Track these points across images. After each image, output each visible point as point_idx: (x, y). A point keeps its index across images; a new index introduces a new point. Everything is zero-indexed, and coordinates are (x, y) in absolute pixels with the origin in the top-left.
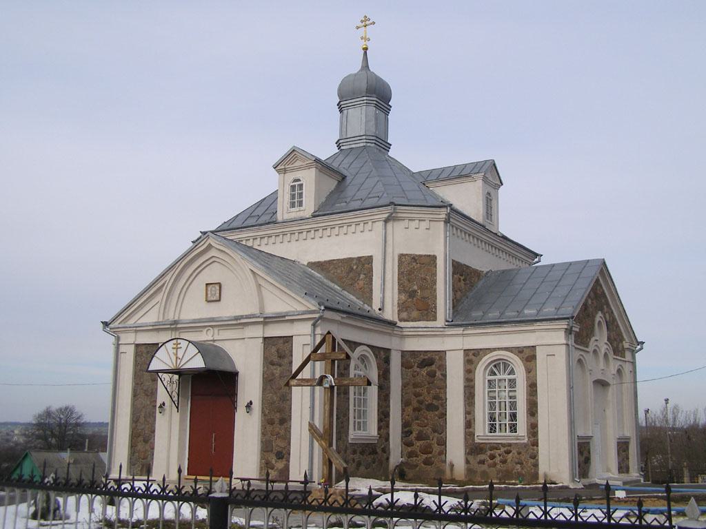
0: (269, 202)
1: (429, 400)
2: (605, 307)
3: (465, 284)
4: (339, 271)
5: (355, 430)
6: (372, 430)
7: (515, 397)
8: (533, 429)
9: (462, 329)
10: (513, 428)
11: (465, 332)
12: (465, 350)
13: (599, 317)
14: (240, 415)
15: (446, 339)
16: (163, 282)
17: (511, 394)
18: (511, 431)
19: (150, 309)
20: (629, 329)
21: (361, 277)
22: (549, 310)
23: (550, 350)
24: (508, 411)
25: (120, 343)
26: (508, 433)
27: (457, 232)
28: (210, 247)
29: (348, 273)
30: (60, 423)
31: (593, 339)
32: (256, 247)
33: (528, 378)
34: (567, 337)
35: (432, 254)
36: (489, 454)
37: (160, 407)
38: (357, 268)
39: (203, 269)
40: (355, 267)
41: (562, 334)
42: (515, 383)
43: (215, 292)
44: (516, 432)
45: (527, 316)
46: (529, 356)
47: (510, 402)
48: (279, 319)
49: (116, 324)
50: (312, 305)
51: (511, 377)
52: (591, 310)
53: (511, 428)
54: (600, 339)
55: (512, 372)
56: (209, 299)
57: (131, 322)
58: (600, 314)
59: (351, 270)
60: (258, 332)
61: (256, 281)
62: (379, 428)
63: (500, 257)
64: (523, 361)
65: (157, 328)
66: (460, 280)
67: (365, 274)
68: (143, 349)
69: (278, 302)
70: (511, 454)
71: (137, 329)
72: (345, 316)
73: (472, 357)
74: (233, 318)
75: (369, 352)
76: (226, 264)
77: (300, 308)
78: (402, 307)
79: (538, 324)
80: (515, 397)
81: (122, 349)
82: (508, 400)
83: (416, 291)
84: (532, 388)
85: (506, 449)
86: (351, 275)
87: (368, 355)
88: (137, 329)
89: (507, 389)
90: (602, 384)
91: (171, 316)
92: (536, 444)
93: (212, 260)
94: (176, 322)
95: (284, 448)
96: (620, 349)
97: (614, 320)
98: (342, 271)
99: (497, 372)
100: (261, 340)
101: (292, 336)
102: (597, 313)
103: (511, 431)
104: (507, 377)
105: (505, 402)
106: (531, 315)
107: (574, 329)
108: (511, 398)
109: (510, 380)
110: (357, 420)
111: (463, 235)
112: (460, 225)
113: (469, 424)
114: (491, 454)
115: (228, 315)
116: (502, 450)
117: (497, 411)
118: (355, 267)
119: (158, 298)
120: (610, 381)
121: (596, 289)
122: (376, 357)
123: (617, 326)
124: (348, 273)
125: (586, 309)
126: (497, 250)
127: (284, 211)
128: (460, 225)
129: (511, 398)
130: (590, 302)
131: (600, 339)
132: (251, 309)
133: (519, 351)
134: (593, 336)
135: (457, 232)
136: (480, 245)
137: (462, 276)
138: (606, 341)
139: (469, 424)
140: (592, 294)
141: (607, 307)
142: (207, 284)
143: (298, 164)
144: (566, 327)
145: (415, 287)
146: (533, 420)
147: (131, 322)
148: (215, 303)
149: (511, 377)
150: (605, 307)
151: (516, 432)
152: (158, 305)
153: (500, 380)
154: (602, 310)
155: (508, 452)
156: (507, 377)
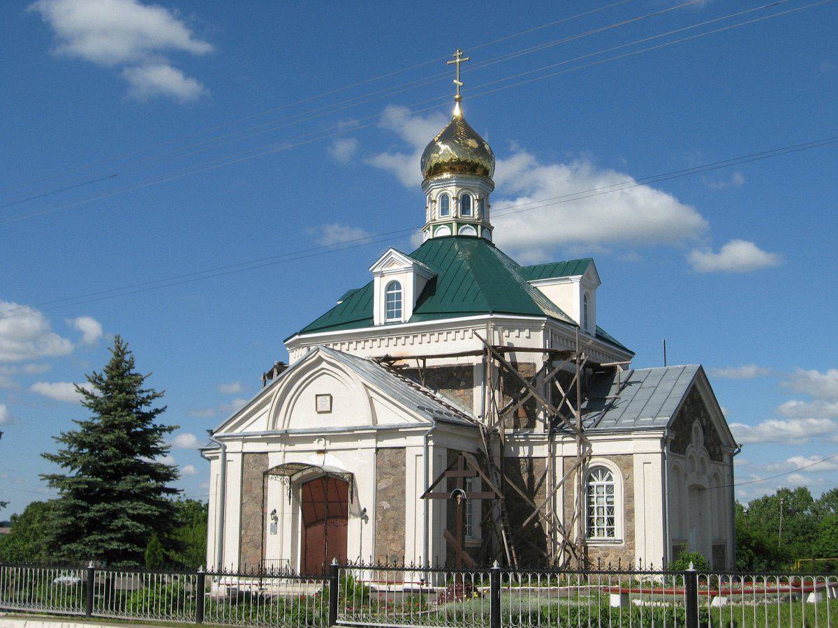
1: (686, 557)
7: (612, 503)
8: (630, 535)
9: (562, 436)
10: (611, 532)
11: (565, 439)
12: (564, 457)
13: (696, 424)
14: (353, 524)
16: (271, 392)
17: (609, 500)
18: (609, 535)
19: (257, 419)
20: (713, 400)
22: (646, 420)
24: (606, 516)
25: (226, 451)
26: (606, 537)
27: (567, 343)
28: (320, 360)
32: (343, 351)
33: (626, 485)
34: (662, 447)
35: (531, 361)
37: (272, 514)
38: (457, 375)
41: (658, 442)
42: (613, 488)
43: (326, 403)
44: (613, 536)
45: (623, 425)
46: (625, 462)
47: (608, 507)
48: (392, 432)
49: (222, 433)
50: (426, 419)
51: (609, 483)
53: (608, 532)
54: (696, 447)
55: (610, 478)
56: (319, 410)
57: (237, 431)
60: (372, 443)
61: (368, 393)
64: (620, 468)
65: (266, 438)
67: (465, 381)
68: (250, 459)
69: (390, 415)
70: (609, 557)
71: (245, 439)
72: (453, 427)
74: (346, 429)
76: (341, 379)
77: (413, 421)
79: (636, 433)
80: (612, 503)
81: (229, 457)
82: (606, 505)
84: (629, 497)
88: (245, 439)
89: (605, 495)
90: (699, 489)
91: (280, 426)
92: (632, 547)
93: (322, 373)
94: (287, 432)
95: (399, 552)
96: (717, 453)
97: (711, 424)
98: (442, 377)
99: (595, 478)
100: (374, 450)
101: (405, 448)
102: (694, 419)
103: (609, 535)
104: (604, 483)
105: (603, 507)
106: (628, 424)
107: (669, 437)
108: (608, 503)
109: (608, 486)
111: (569, 343)
115: (339, 426)
116: (601, 552)
117: (596, 516)
118: (455, 374)
119: (268, 407)
120: (706, 485)
121: (693, 395)
123: (715, 431)
125: (682, 415)
126: (597, 353)
129: (608, 503)
131: (696, 447)
132: (363, 420)
135: (567, 343)
142: (317, 396)
143: (395, 267)
144: (662, 436)
146: (629, 524)
147: (237, 431)
149: (609, 483)
150: (702, 411)
151: (613, 536)
152: (267, 413)
153: (598, 486)
154: (699, 415)
155: (606, 556)
156: (604, 483)
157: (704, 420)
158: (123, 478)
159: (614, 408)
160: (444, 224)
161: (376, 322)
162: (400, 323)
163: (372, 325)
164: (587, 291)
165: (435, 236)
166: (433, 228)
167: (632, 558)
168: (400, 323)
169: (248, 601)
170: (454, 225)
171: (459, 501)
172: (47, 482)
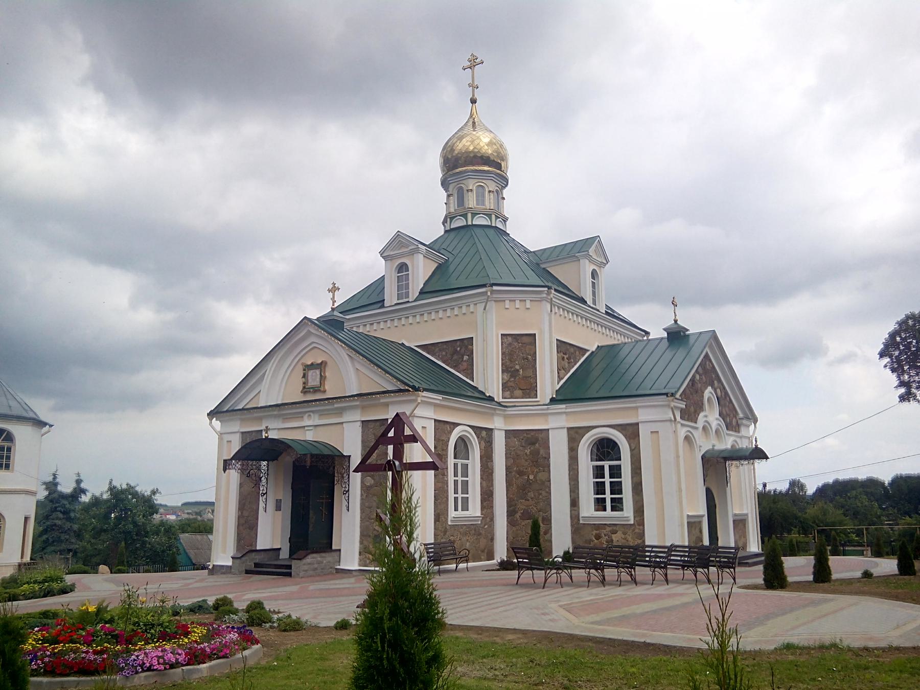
0: (378, 285)
2: (716, 382)
3: (569, 363)
4: (444, 353)
5: (456, 509)
6: (475, 510)
8: (639, 510)
13: (708, 392)
15: (550, 418)
21: (464, 359)
23: (655, 426)
27: (573, 318)
29: (452, 355)
30: (147, 534)
31: (702, 415)
36: (594, 534)
38: (460, 349)
39: (494, 181)
40: (458, 349)
52: (699, 385)
54: (711, 416)
58: (710, 388)
59: (455, 352)
62: (482, 508)
63: (595, 330)
66: (563, 358)
73: (575, 435)
75: (471, 435)
78: (505, 387)
83: (518, 370)
85: (611, 528)
86: (455, 357)
87: (468, 435)
98: (447, 353)
102: (706, 388)
110: (460, 496)
112: (616, 327)
113: (574, 503)
114: (596, 534)
118: (458, 349)
122: (478, 438)
124: (452, 355)
125: (693, 385)
127: (391, 297)
128: (616, 327)
130: (698, 377)
133: (620, 428)
134: (703, 411)
136: (616, 336)
137: (565, 354)
138: (718, 416)
139: (574, 503)
140: (700, 370)
141: (718, 382)
145: (517, 367)
148: (290, 430)
155: (615, 532)
157: (718, 390)
158: (314, 517)
159: (302, 377)
160: (459, 216)
161: (387, 303)
162: (408, 302)
163: (383, 306)
164: (595, 268)
165: (451, 227)
166: (472, 216)
167: (642, 535)
168: (408, 302)
169: (155, 570)
170: (469, 215)
171: (857, 538)
172: (50, 479)
